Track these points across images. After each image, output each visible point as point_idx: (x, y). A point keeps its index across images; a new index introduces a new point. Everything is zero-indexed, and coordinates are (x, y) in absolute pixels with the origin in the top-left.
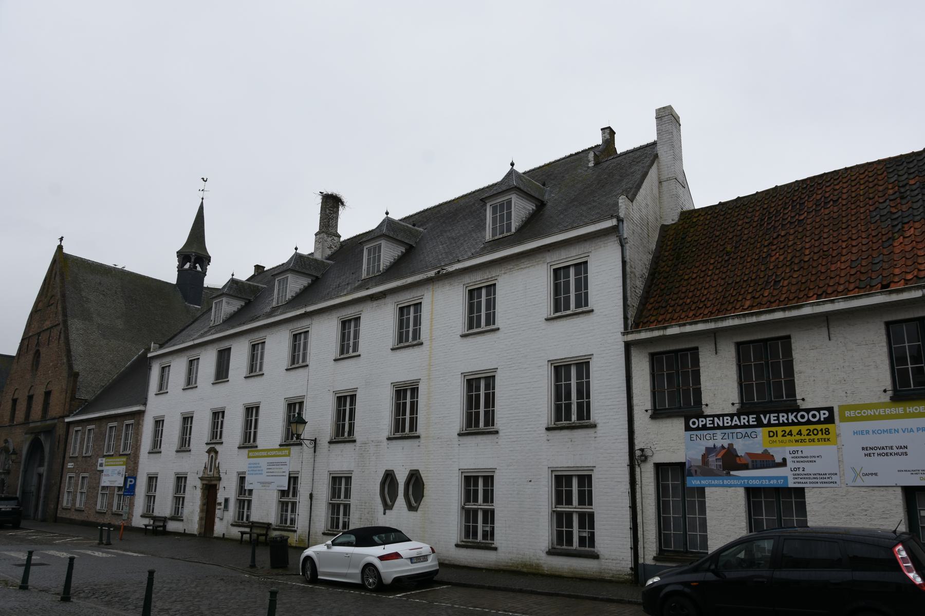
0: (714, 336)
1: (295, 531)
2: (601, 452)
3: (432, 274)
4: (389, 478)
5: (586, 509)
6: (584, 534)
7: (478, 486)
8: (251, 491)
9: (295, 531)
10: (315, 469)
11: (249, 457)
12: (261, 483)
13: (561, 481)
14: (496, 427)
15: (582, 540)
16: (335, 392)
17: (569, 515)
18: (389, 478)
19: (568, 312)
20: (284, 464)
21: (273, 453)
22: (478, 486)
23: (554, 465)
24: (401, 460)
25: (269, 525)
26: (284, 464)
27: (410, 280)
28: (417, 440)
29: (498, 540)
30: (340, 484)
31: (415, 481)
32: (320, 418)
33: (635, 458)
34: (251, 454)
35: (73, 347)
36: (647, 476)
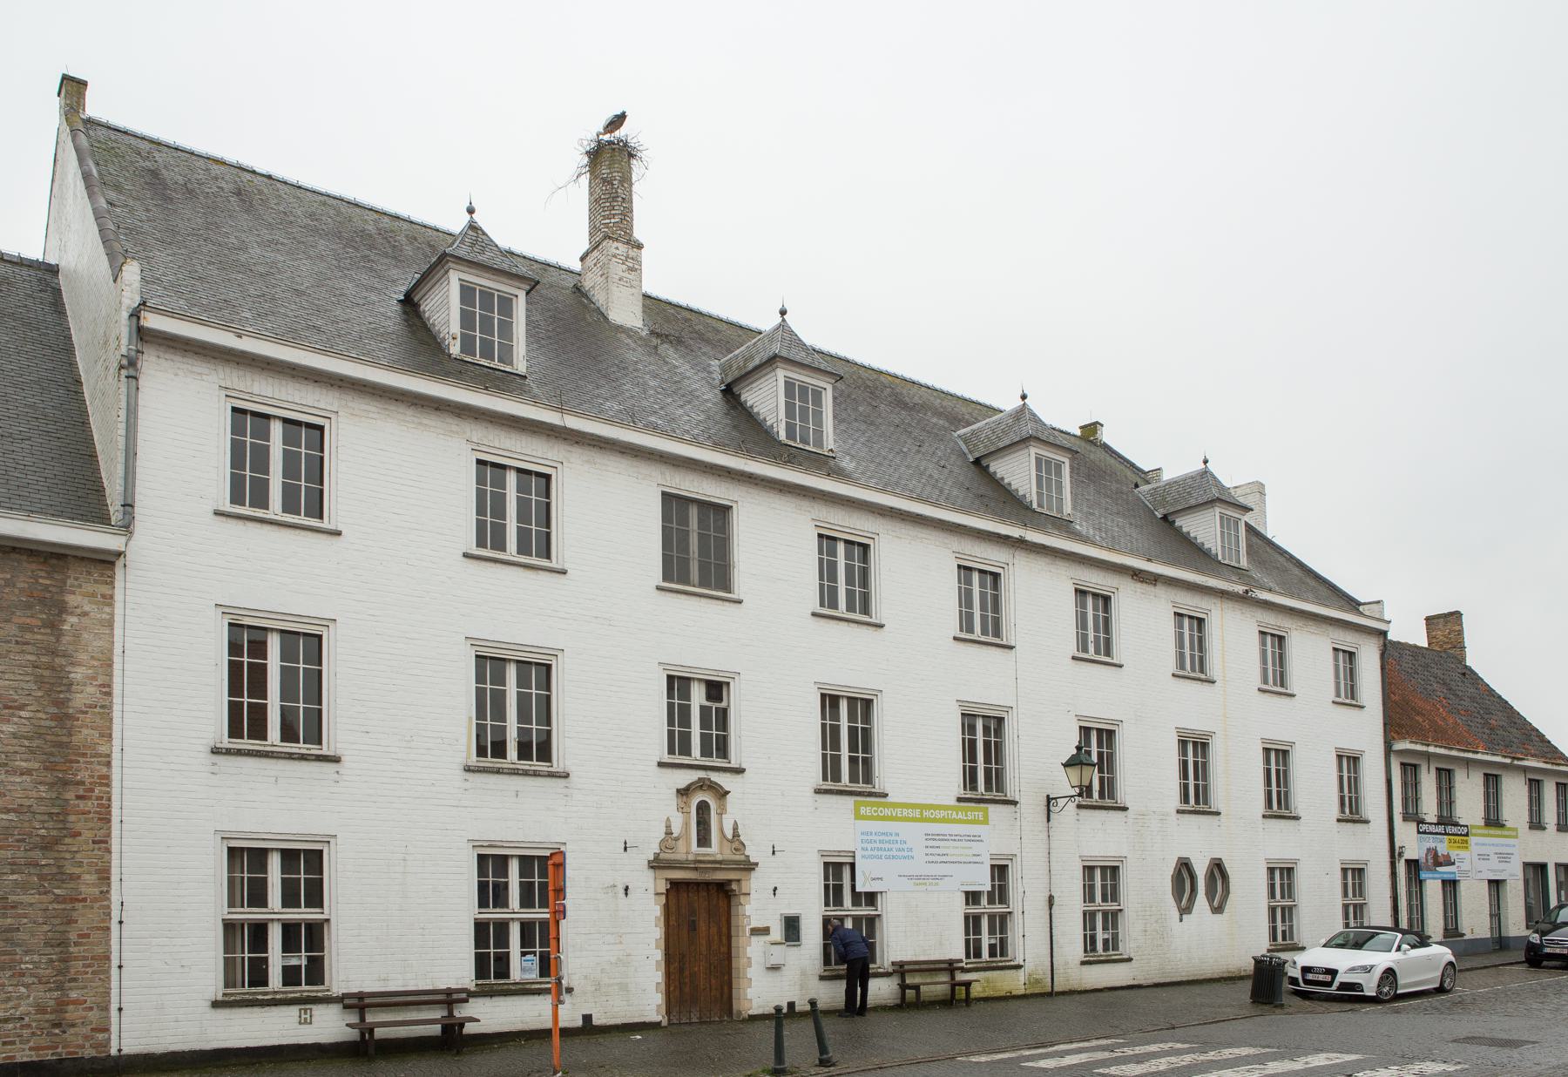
0: (1468, 763)
1: (1019, 967)
2: (1368, 845)
3: (1240, 589)
4: (1184, 869)
5: (303, 914)
6: (294, 962)
7: (1282, 877)
8: (871, 898)
9: (1019, 967)
10: (1049, 856)
11: (858, 816)
12: (910, 877)
13: (246, 861)
14: (558, 764)
15: (291, 976)
16: (1079, 718)
17: (502, 927)
18: (1184, 869)
19: (260, 513)
20: (977, 839)
21: (943, 813)
22: (1282, 877)
23: (230, 826)
24: (1198, 842)
25: (951, 962)
26: (977, 839)
27: (573, 422)
28: (561, 782)
29: (1126, 948)
30: (1103, 879)
31: (1218, 869)
32: (1038, 757)
33: (1394, 853)
34: (863, 810)
35: (798, 358)
36: (1401, 868)
